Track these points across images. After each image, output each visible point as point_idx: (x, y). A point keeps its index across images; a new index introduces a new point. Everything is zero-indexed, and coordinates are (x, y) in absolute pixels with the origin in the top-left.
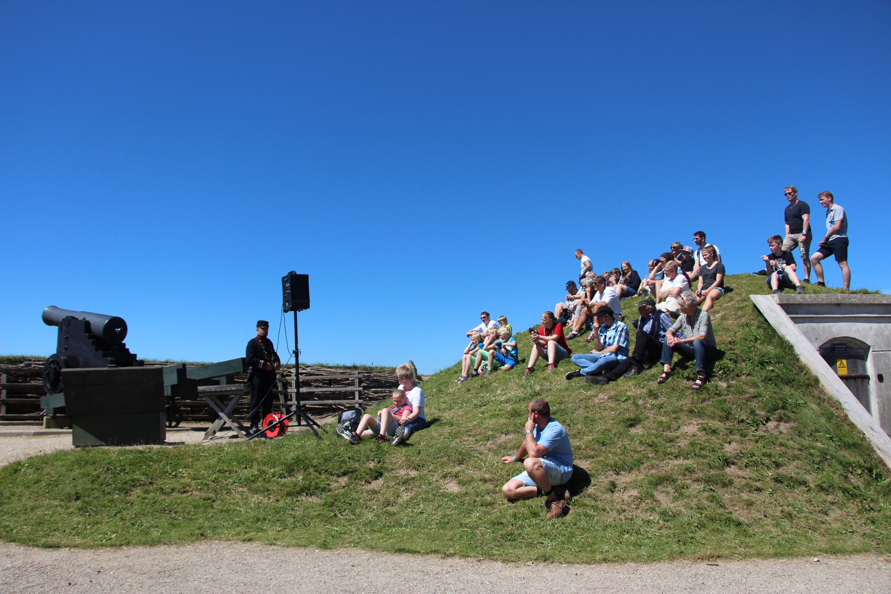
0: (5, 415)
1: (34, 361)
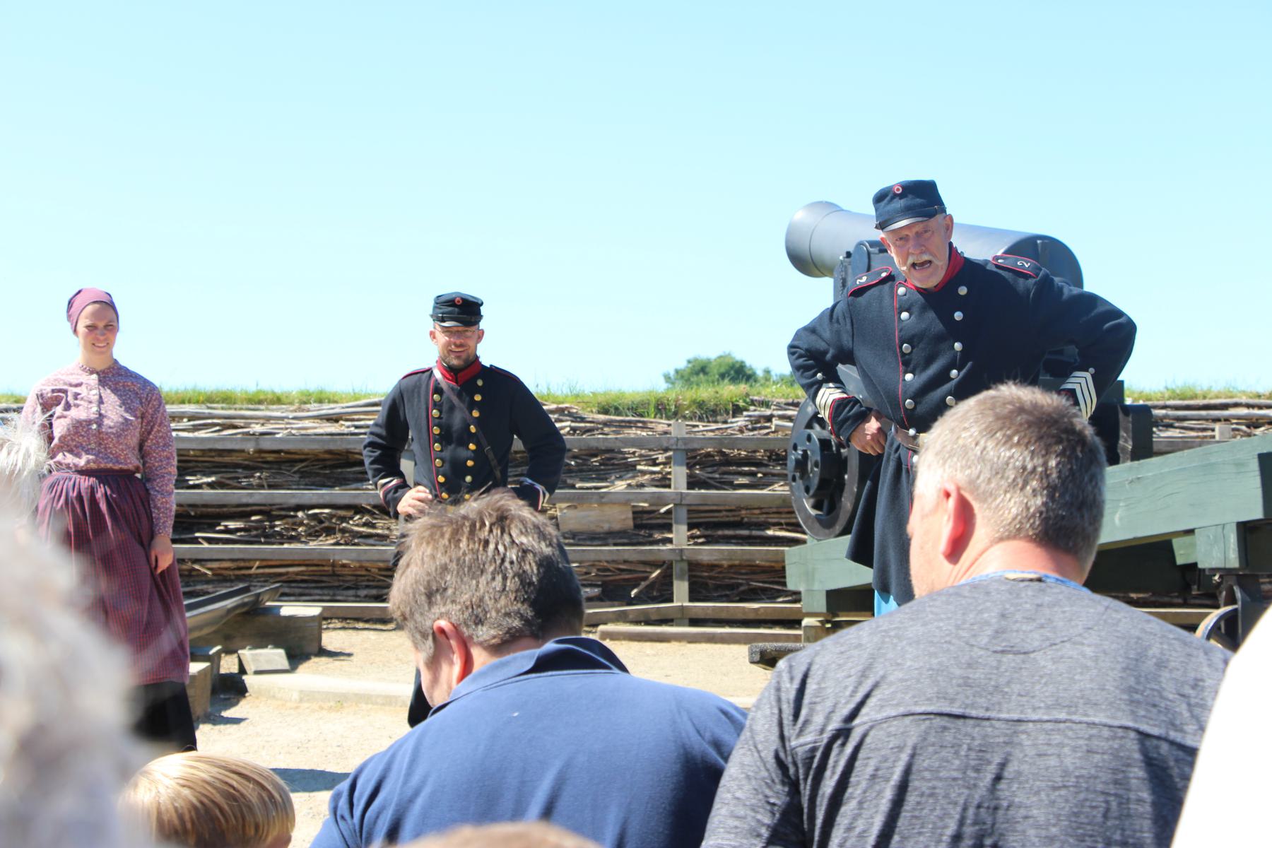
0: (786, 549)
1: (779, 407)
